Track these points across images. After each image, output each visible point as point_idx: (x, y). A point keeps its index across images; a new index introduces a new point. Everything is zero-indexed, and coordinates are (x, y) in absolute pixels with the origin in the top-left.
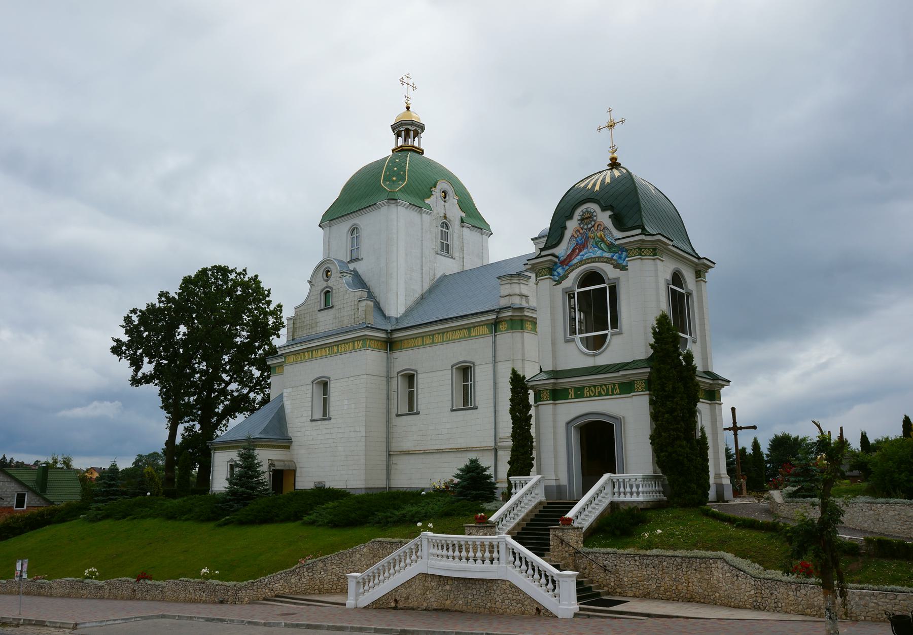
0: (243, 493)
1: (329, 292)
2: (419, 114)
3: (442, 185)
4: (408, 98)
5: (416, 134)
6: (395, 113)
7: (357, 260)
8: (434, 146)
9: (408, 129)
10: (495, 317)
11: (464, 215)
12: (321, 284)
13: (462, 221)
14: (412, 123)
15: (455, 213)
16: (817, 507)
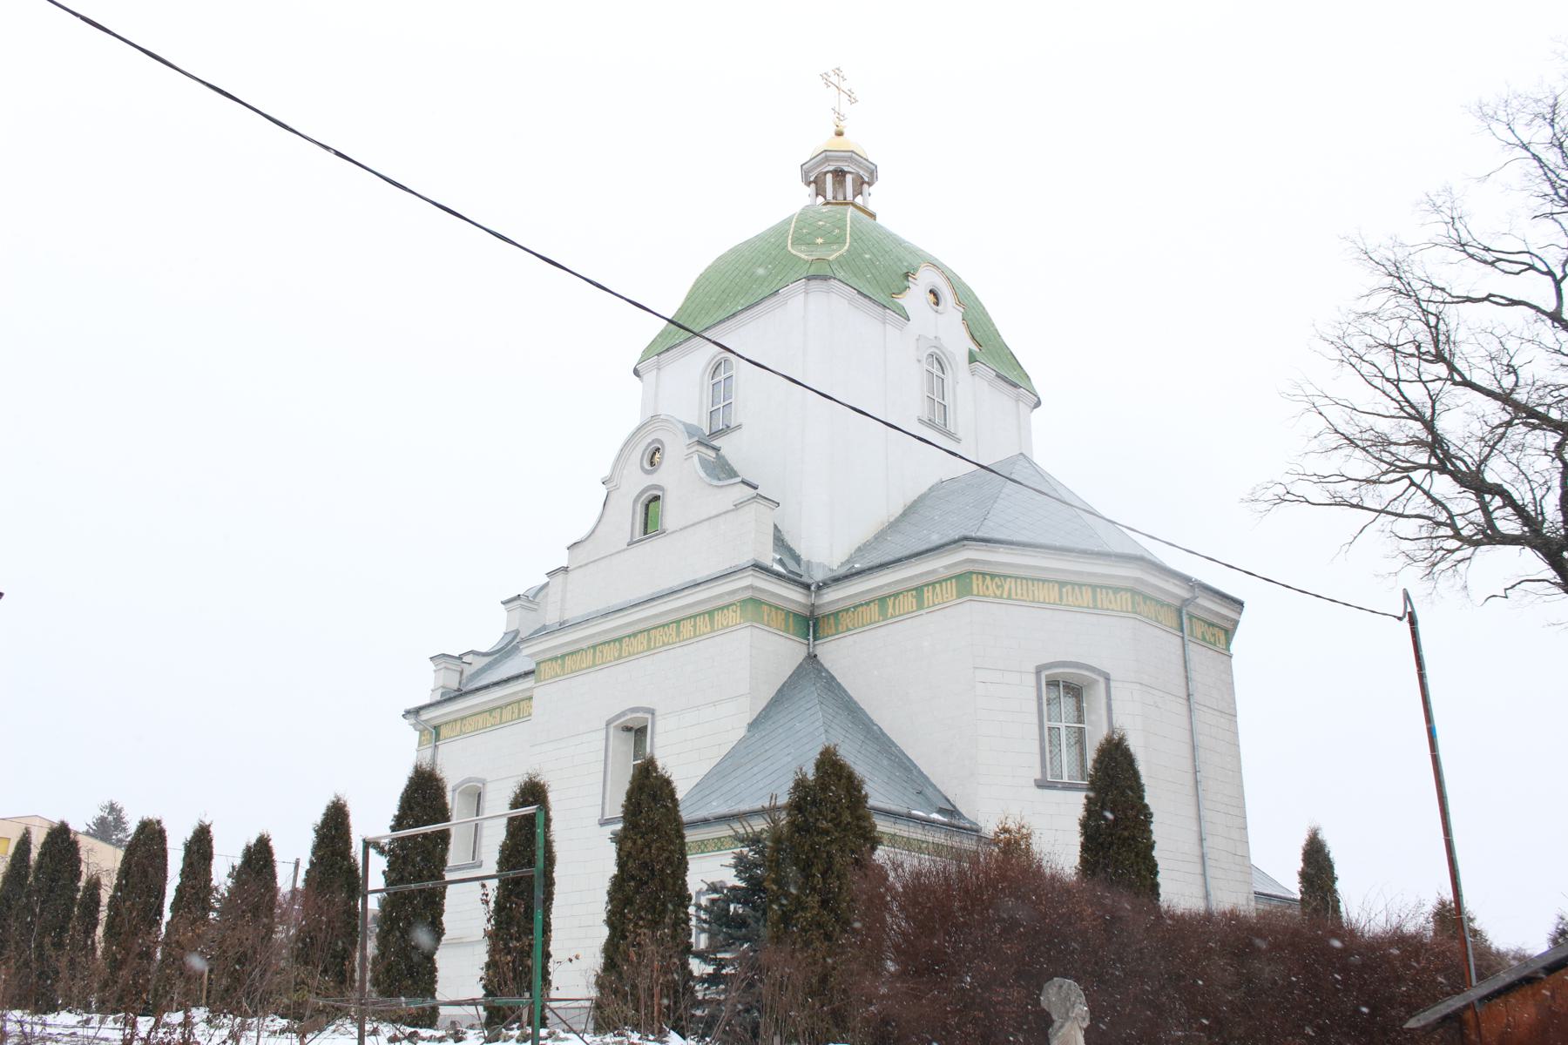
0: (28, 867)
1: (657, 498)
2: (863, 140)
3: (925, 278)
4: (840, 117)
5: (860, 184)
6: (818, 139)
7: (727, 430)
8: (894, 208)
9: (839, 176)
10: (1186, 594)
11: (975, 348)
12: (636, 482)
13: (972, 359)
14: (852, 156)
15: (958, 343)
16: (381, 1027)
